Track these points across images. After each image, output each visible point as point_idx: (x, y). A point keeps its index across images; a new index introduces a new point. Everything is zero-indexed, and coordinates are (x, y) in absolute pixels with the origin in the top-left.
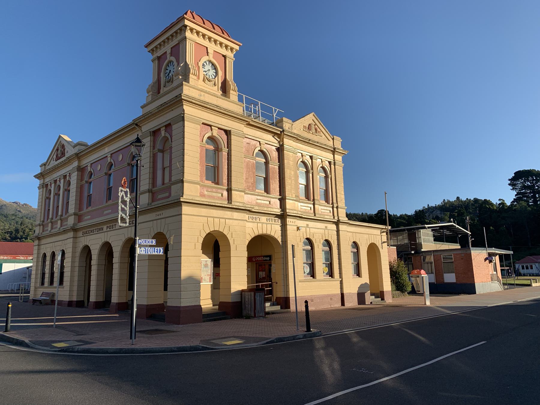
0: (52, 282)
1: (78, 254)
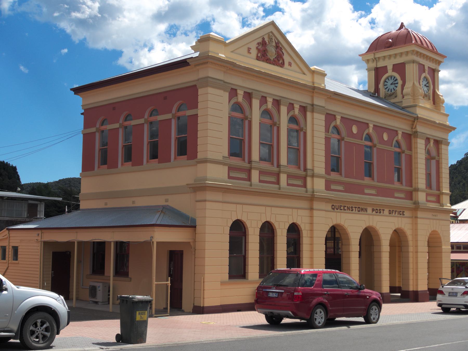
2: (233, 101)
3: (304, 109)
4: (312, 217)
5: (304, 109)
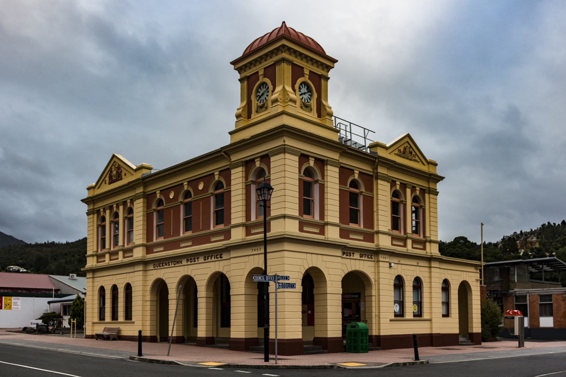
0: (114, 317)
1: (149, 288)
2: (413, 195)
3: (423, 191)
4: (430, 272)
5: (423, 191)
